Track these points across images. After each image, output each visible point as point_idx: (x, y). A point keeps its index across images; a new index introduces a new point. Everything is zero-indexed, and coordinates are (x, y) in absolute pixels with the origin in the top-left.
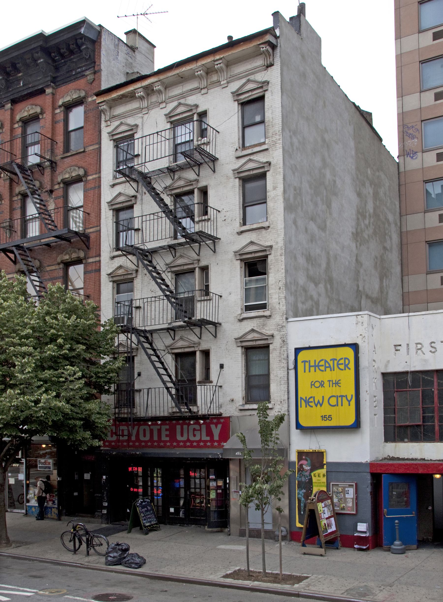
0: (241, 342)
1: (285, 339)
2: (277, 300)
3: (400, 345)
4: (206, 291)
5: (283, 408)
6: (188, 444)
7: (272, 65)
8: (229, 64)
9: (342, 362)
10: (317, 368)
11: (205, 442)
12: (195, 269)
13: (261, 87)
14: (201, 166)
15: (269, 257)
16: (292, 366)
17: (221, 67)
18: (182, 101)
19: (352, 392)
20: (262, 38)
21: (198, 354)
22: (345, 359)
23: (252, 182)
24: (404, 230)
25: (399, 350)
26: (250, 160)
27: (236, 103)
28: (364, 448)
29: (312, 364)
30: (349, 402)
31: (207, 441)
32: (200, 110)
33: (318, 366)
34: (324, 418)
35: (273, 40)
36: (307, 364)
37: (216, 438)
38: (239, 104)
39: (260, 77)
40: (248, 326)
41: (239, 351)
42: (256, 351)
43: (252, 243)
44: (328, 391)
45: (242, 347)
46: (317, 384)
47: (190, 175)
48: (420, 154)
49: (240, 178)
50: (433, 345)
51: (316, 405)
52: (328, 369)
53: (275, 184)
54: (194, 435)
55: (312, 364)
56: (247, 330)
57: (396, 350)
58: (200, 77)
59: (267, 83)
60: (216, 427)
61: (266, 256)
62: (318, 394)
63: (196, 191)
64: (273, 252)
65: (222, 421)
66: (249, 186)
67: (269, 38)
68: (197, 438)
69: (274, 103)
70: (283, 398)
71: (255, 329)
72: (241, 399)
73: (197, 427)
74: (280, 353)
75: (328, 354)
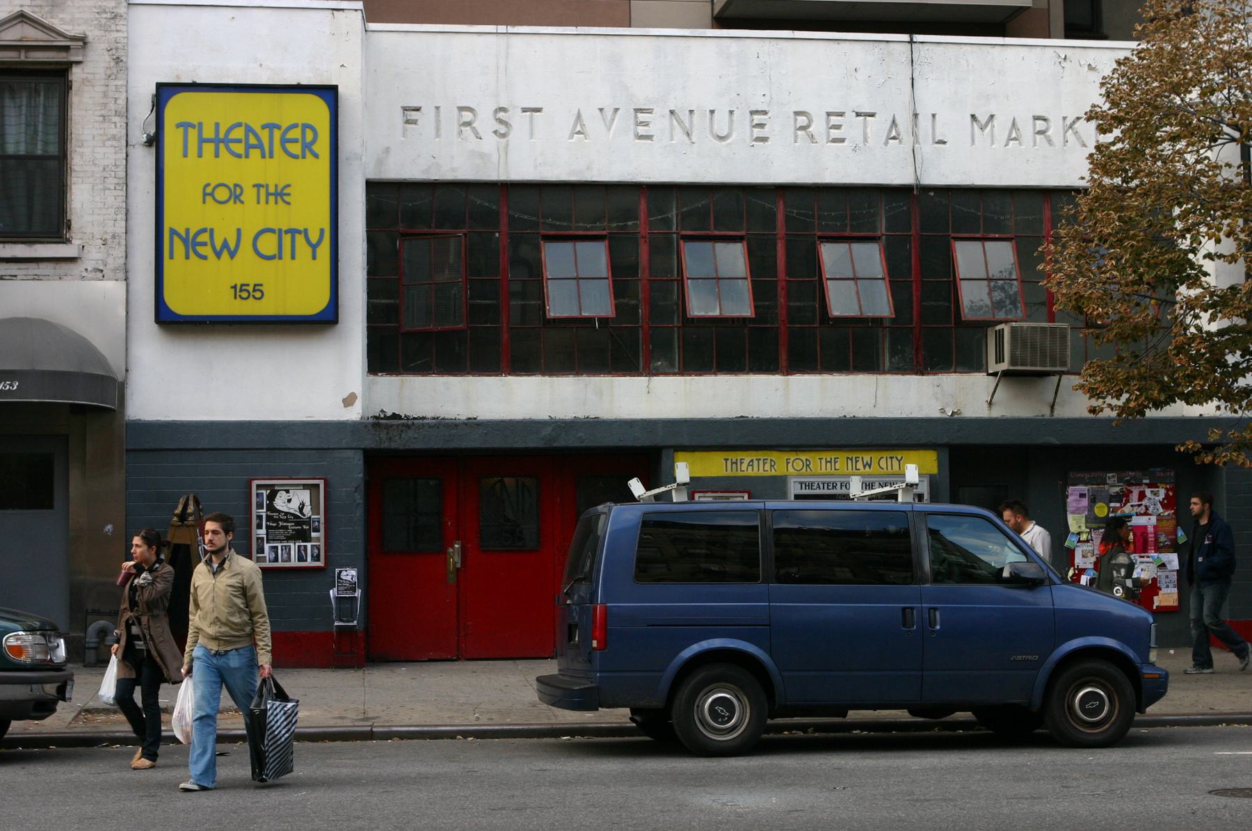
1: (121, 53)
3: (418, 109)
5: (110, 261)
9: (295, 134)
10: (222, 146)
22: (306, 126)
25: (415, 122)
28: (328, 385)
30: (314, 247)
33: (227, 141)
34: (240, 291)
36: (193, 134)
44: (253, 215)
46: (222, 194)
50: (501, 115)
51: (218, 255)
52: (255, 153)
55: (208, 133)
57: (408, 122)
70: (110, 230)
71: (27, 10)
74: (105, 95)
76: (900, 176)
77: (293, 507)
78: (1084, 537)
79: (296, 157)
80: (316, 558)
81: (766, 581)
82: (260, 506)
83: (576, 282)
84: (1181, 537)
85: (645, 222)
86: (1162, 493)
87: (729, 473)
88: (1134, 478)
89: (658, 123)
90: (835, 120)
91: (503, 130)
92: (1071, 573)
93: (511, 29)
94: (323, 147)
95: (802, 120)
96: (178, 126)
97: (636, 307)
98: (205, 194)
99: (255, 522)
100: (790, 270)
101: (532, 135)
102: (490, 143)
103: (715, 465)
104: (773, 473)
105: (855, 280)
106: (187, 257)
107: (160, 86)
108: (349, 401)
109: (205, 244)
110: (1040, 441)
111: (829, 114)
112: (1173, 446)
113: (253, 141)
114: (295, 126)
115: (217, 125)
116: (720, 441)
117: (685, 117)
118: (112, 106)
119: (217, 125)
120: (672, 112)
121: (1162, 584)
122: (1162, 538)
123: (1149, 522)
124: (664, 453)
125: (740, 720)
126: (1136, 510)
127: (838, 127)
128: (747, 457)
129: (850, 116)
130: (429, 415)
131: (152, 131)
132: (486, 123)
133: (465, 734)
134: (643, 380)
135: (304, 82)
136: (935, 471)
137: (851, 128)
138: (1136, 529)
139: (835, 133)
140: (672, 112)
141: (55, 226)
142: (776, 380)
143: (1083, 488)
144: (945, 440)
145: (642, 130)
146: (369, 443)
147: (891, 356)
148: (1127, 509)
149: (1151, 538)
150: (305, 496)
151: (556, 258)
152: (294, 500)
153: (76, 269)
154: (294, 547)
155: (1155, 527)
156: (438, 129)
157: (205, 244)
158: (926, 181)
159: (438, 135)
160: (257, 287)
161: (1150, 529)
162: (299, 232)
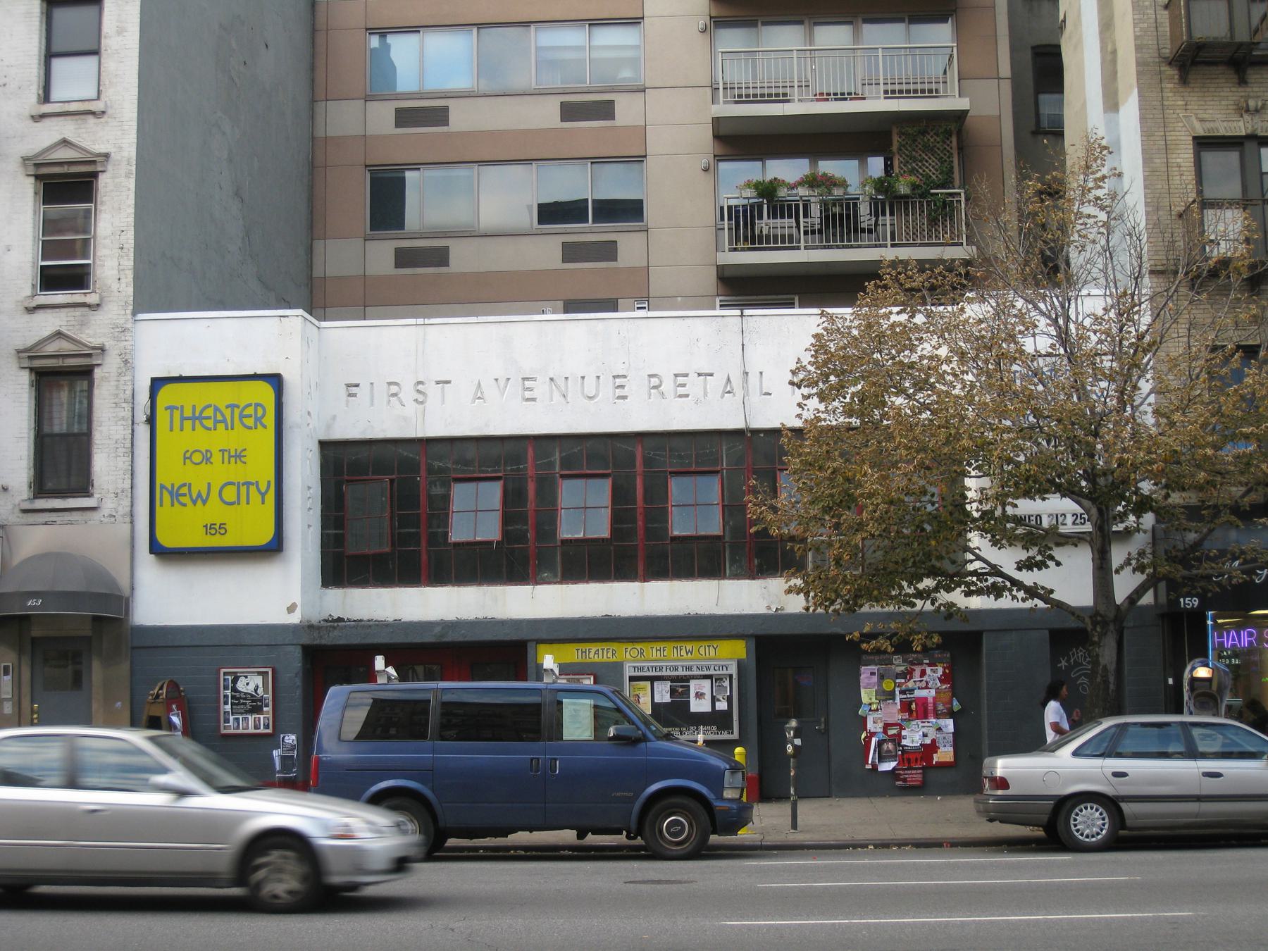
0: (30, 358)
1: (128, 356)
2: (116, 272)
3: (357, 386)
5: (120, 509)
9: (250, 411)
22: (257, 405)
25: (354, 395)
28: (280, 595)
30: (263, 495)
33: (201, 418)
34: (210, 529)
41: (25, 378)
44: (219, 472)
46: (197, 458)
50: (420, 387)
51: (194, 502)
52: (221, 426)
57: (350, 395)
61: (95, 175)
62: (198, 478)
64: (110, 168)
70: (120, 486)
71: (64, 330)
74: (117, 387)
76: (735, 423)
77: (250, 689)
78: (874, 707)
79: (250, 428)
80: (266, 727)
81: (432, 739)
82: (226, 688)
83: (475, 514)
84: (956, 706)
86: (940, 671)
87: (580, 660)
88: (916, 659)
89: (540, 388)
90: (680, 380)
91: (421, 398)
93: (427, 321)
94: (270, 420)
95: (655, 381)
96: (167, 408)
97: (527, 531)
98: (185, 458)
100: (645, 500)
101: (443, 402)
102: (411, 409)
103: (572, 654)
106: (173, 505)
108: (291, 609)
109: (184, 495)
110: (829, 631)
111: (676, 375)
112: (843, 636)
113: (219, 417)
114: (250, 405)
115: (194, 407)
116: (571, 636)
117: (561, 382)
118: (122, 395)
119: (194, 407)
120: (552, 379)
121: (940, 744)
122: (940, 707)
123: (929, 694)
126: (918, 684)
127: (683, 385)
128: (594, 647)
129: (693, 376)
130: (366, 618)
131: (148, 412)
132: (408, 393)
134: (529, 588)
135: (259, 372)
136: (744, 656)
137: (694, 386)
138: (918, 700)
139: (681, 390)
140: (552, 379)
141: (84, 488)
142: (635, 586)
143: (874, 668)
145: (528, 394)
146: (306, 640)
147: (731, 565)
148: (910, 684)
149: (930, 707)
150: (258, 680)
151: (461, 495)
152: (251, 683)
153: (96, 516)
154: (251, 718)
155: (934, 698)
156: (372, 400)
157: (184, 495)
159: (372, 404)
160: (222, 526)
161: (930, 700)
162: (252, 484)
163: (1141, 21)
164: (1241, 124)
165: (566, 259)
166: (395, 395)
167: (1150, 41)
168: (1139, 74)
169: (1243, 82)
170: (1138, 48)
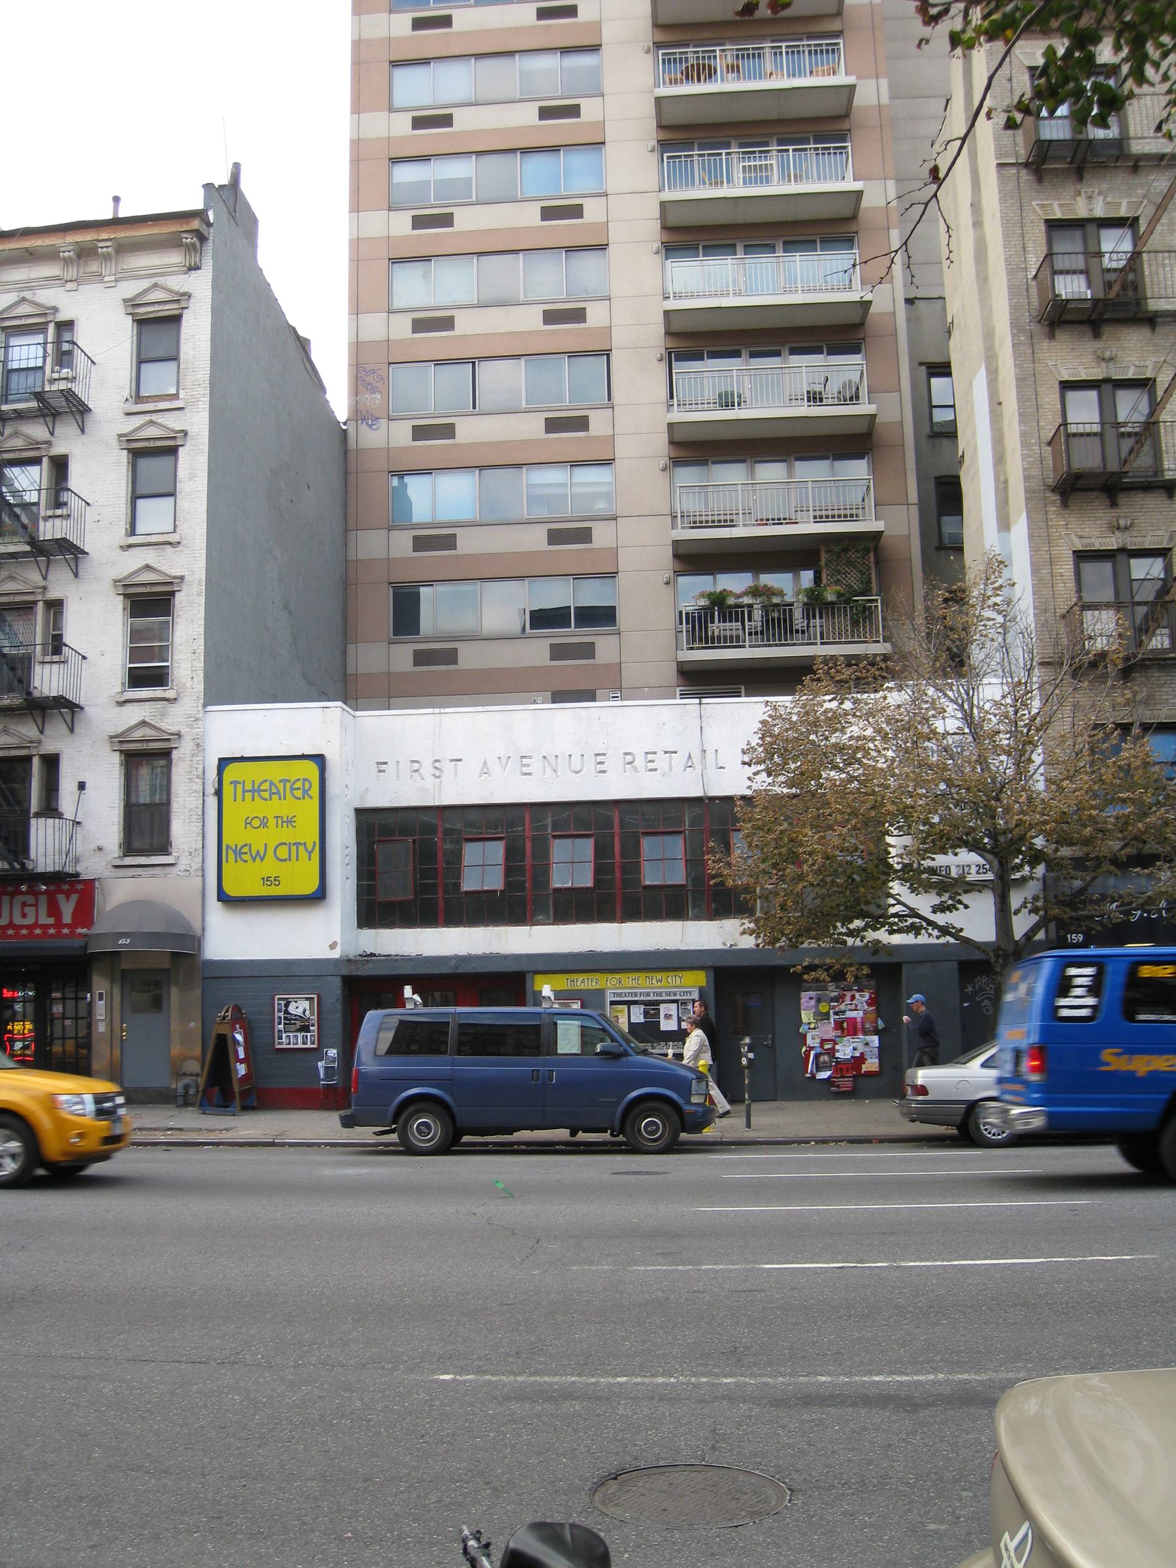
2: (189, 672)
4: (57, 645)
6: (10, 932)
7: (197, 268)
8: (122, 249)
9: (299, 785)
11: (45, 927)
12: (35, 602)
13: (178, 301)
14: (58, 419)
15: (177, 595)
16: (211, 789)
17: (108, 253)
18: (27, 294)
19: (314, 836)
20: (187, 223)
21: (36, 761)
22: (305, 780)
23: (150, 456)
24: (351, 557)
25: (383, 771)
26: (152, 422)
27: (130, 317)
28: (324, 935)
29: (249, 787)
30: (310, 853)
31: (48, 926)
32: (62, 317)
33: (259, 791)
34: (266, 880)
35: (204, 229)
36: (239, 787)
37: (67, 919)
38: (134, 320)
39: (179, 283)
40: (134, 714)
41: (116, 758)
42: (145, 759)
43: (148, 567)
44: (274, 835)
45: (121, 751)
46: (256, 823)
47: (38, 431)
48: (384, 422)
49: (129, 450)
50: (437, 764)
51: (254, 859)
52: (275, 797)
53: (193, 468)
54: (24, 916)
55: (249, 787)
56: (133, 722)
58: (67, 262)
59: (188, 296)
60: (68, 899)
61: (173, 593)
62: (257, 839)
63: (45, 461)
64: (184, 588)
65: (79, 887)
66: (144, 464)
67: (196, 224)
68: (30, 921)
69: (196, 334)
70: (194, 846)
71: (147, 719)
72: (116, 848)
73: (30, 899)
75: (275, 772)
77: (299, 1012)
78: (812, 1026)
82: (280, 1011)
83: (482, 867)
84: (881, 1024)
85: (522, 828)
86: (867, 995)
87: (569, 988)
89: (535, 765)
90: (650, 757)
91: (437, 773)
92: (804, 1049)
93: (442, 710)
94: (315, 792)
95: (629, 758)
99: (276, 1021)
102: (429, 782)
103: (563, 982)
104: (598, 987)
105: (663, 863)
107: (221, 760)
108: (333, 946)
117: (552, 760)
122: (868, 1026)
123: (858, 1015)
124: (528, 976)
125: (436, 1131)
127: (653, 761)
128: (580, 977)
129: (660, 754)
132: (427, 769)
133: (327, 1144)
136: (704, 984)
137: (661, 761)
139: (651, 766)
144: (710, 964)
145: (525, 770)
146: (345, 971)
147: (693, 908)
149: (859, 1026)
151: (472, 853)
152: (300, 1007)
154: (300, 1035)
158: (711, 793)
161: (859, 1020)
163: (1029, 456)
164: (1113, 540)
165: (553, 658)
166: (416, 771)
167: (1036, 472)
168: (1027, 499)
169: (1114, 504)
170: (1026, 478)
